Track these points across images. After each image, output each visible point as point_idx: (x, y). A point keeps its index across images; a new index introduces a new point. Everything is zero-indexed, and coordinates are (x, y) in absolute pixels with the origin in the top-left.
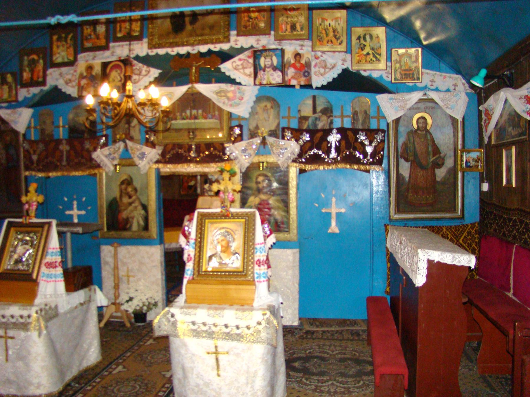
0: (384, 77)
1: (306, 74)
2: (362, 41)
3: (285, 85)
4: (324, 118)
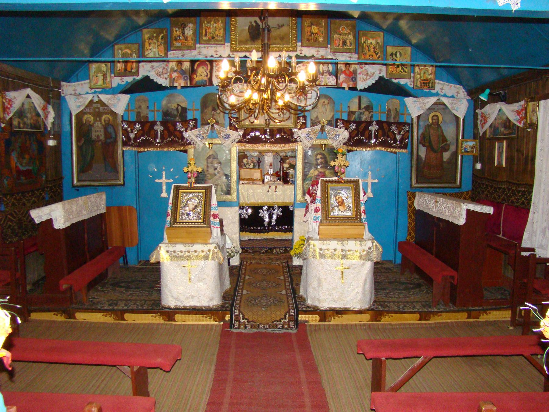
0: (409, 84)
1: (354, 80)
2: (394, 57)
3: (338, 87)
4: (367, 113)
